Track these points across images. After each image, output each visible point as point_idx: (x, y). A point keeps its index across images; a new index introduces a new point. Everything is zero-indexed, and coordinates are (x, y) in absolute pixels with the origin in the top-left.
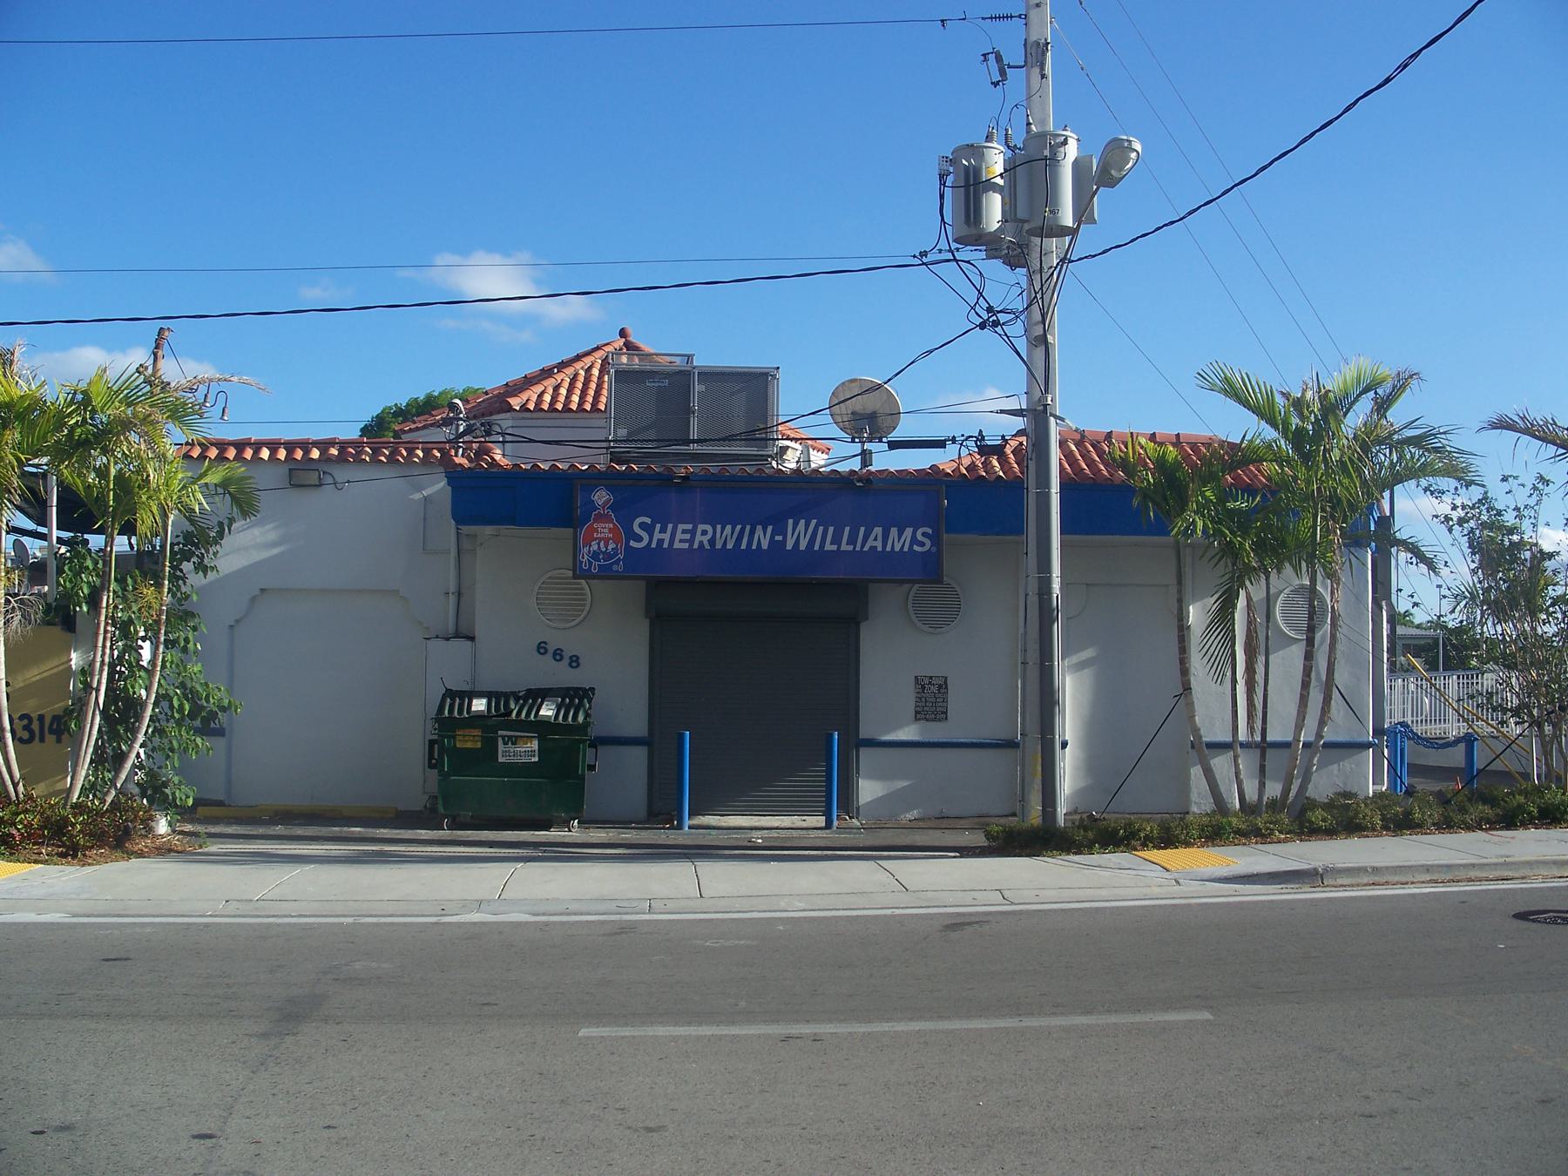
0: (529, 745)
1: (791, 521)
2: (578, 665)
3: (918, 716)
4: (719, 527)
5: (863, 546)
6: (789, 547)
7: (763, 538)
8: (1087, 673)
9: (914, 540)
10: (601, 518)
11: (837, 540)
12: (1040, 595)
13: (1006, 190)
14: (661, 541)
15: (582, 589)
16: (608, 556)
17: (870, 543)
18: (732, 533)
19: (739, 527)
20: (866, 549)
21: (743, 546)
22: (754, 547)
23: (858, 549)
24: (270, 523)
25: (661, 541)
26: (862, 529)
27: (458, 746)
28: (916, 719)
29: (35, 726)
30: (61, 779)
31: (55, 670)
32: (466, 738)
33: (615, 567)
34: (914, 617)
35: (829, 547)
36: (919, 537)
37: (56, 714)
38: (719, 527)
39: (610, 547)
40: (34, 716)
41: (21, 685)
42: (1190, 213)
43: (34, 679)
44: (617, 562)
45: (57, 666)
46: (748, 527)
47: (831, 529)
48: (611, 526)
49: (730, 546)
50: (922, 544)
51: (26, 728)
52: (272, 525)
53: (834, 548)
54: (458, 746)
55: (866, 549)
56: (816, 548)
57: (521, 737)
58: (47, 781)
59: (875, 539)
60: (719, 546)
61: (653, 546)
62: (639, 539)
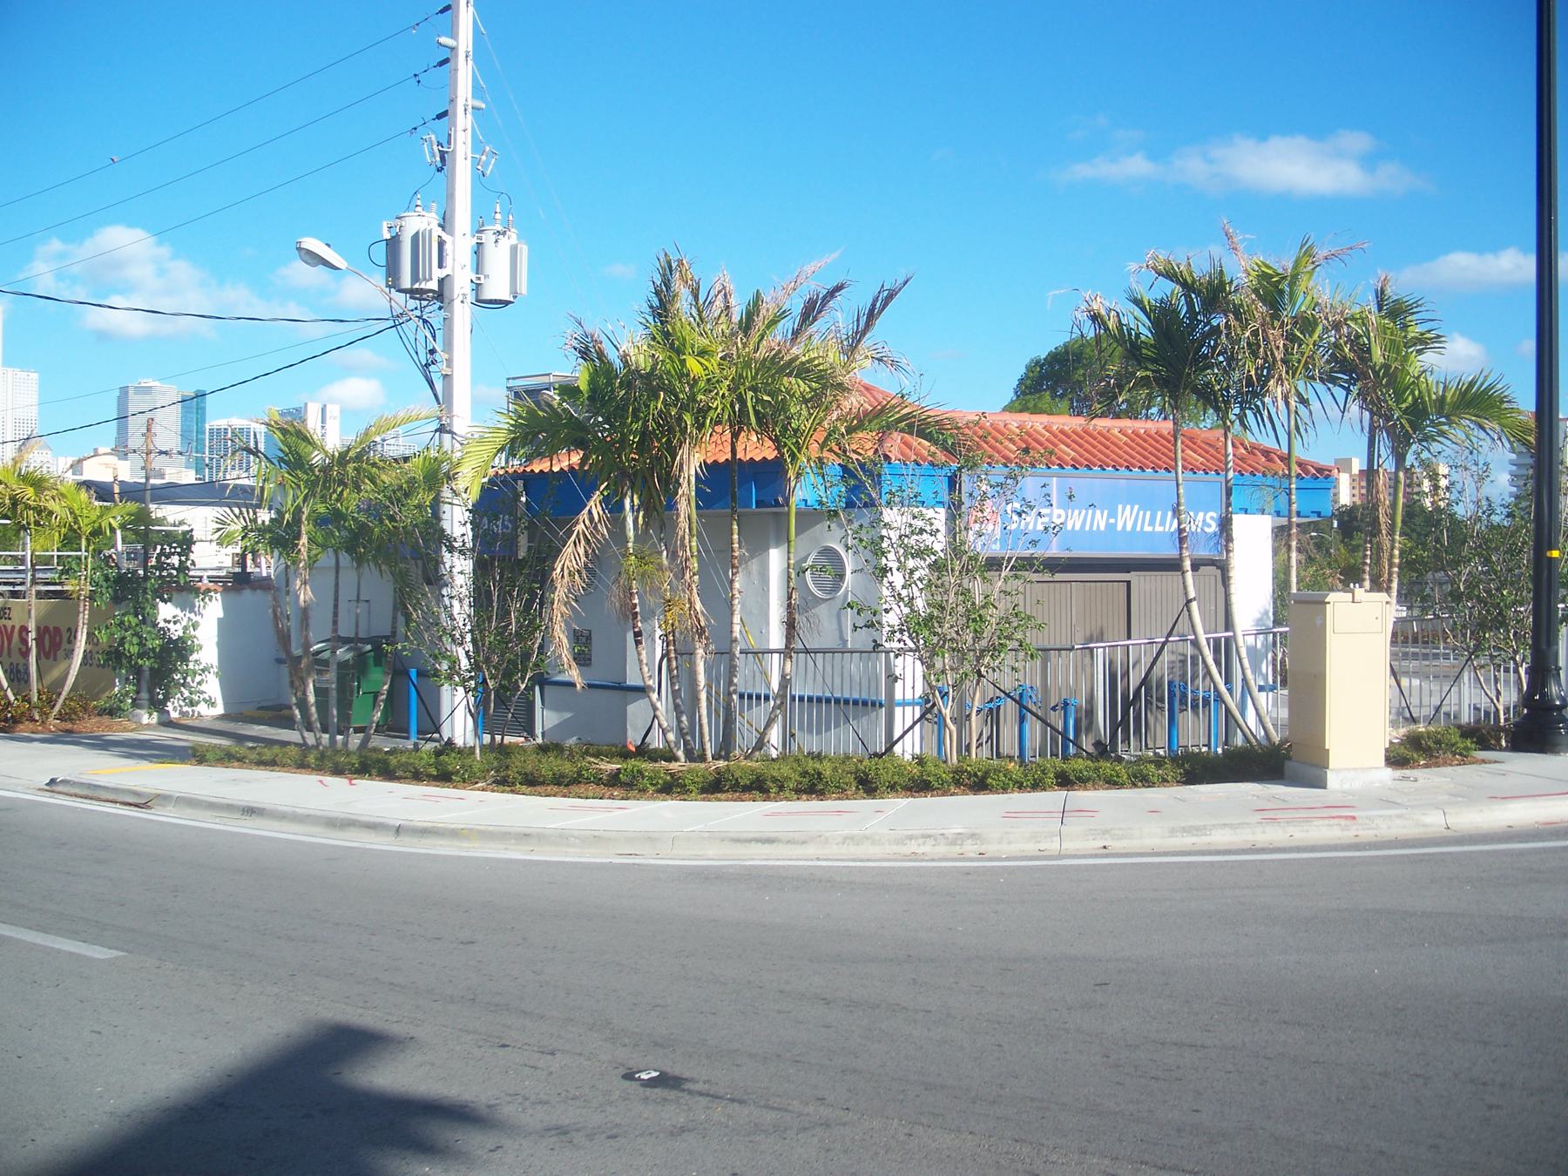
11: (1152, 523)
23: (1167, 530)
35: (1147, 528)
36: (1209, 520)
42: (337, 585)
53: (1150, 529)
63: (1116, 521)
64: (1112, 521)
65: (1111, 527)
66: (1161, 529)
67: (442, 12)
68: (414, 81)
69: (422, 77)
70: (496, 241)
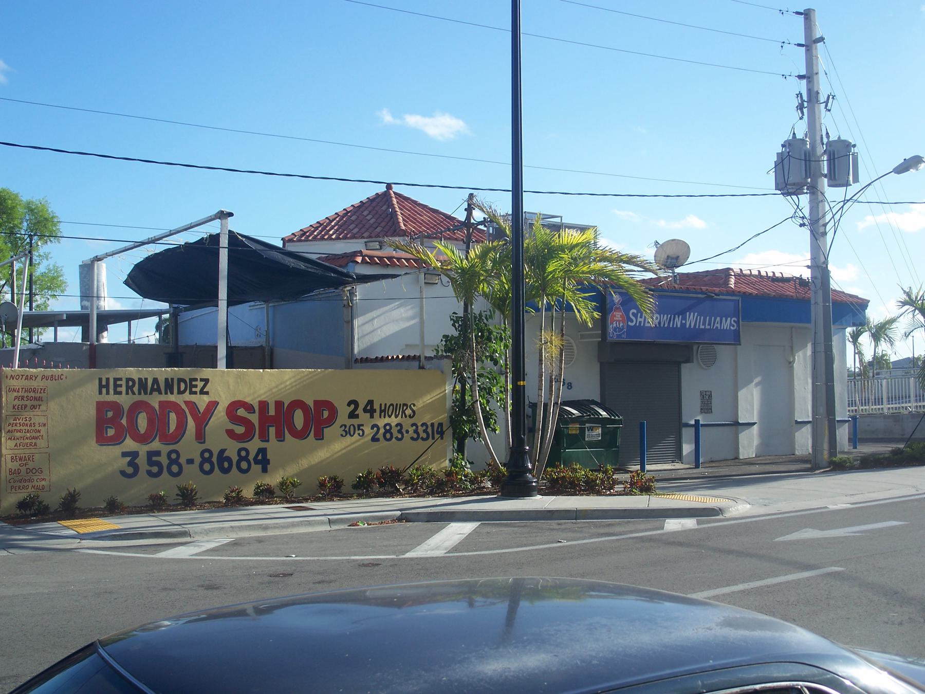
0: (598, 431)
1: (688, 313)
2: (571, 388)
3: (702, 411)
4: (662, 315)
5: (713, 327)
6: (687, 326)
7: (678, 322)
8: (759, 388)
9: (731, 325)
10: (617, 309)
11: (704, 324)
12: (826, 352)
13: (828, 176)
14: (640, 322)
15: (572, 346)
16: (620, 330)
17: (716, 325)
18: (667, 319)
19: (669, 316)
20: (714, 328)
21: (671, 326)
22: (675, 326)
23: (712, 328)
24: (409, 305)
25: (640, 322)
26: (713, 318)
27: (569, 433)
28: (701, 413)
29: (430, 430)
30: (444, 461)
31: (439, 396)
32: (573, 428)
33: (623, 336)
34: (701, 363)
35: (702, 327)
37: (439, 422)
38: (662, 315)
39: (621, 325)
40: (429, 424)
41: (422, 405)
43: (428, 402)
44: (624, 333)
45: (440, 394)
46: (673, 316)
47: (702, 318)
48: (621, 313)
49: (666, 326)
50: (734, 326)
51: (425, 431)
52: (410, 307)
53: (703, 327)
54: (569, 433)
55: (714, 328)
56: (697, 327)
57: (595, 426)
58: (437, 463)
59: (718, 323)
60: (662, 325)
61: (638, 325)
62: (632, 321)
63: (686, 322)
64: (684, 322)
65: (683, 325)
66: (709, 327)
67: (903, 168)
68: (781, 44)
69: (785, 45)
70: (782, 47)
